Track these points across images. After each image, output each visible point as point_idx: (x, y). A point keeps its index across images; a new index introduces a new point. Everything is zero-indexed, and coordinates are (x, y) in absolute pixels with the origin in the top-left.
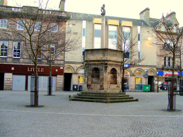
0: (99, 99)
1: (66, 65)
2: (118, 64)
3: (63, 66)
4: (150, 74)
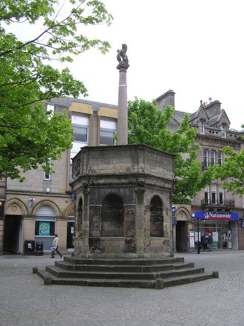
0: (108, 277)
1: (9, 197)
2: (167, 185)
3: (3, 200)
4: (182, 218)
